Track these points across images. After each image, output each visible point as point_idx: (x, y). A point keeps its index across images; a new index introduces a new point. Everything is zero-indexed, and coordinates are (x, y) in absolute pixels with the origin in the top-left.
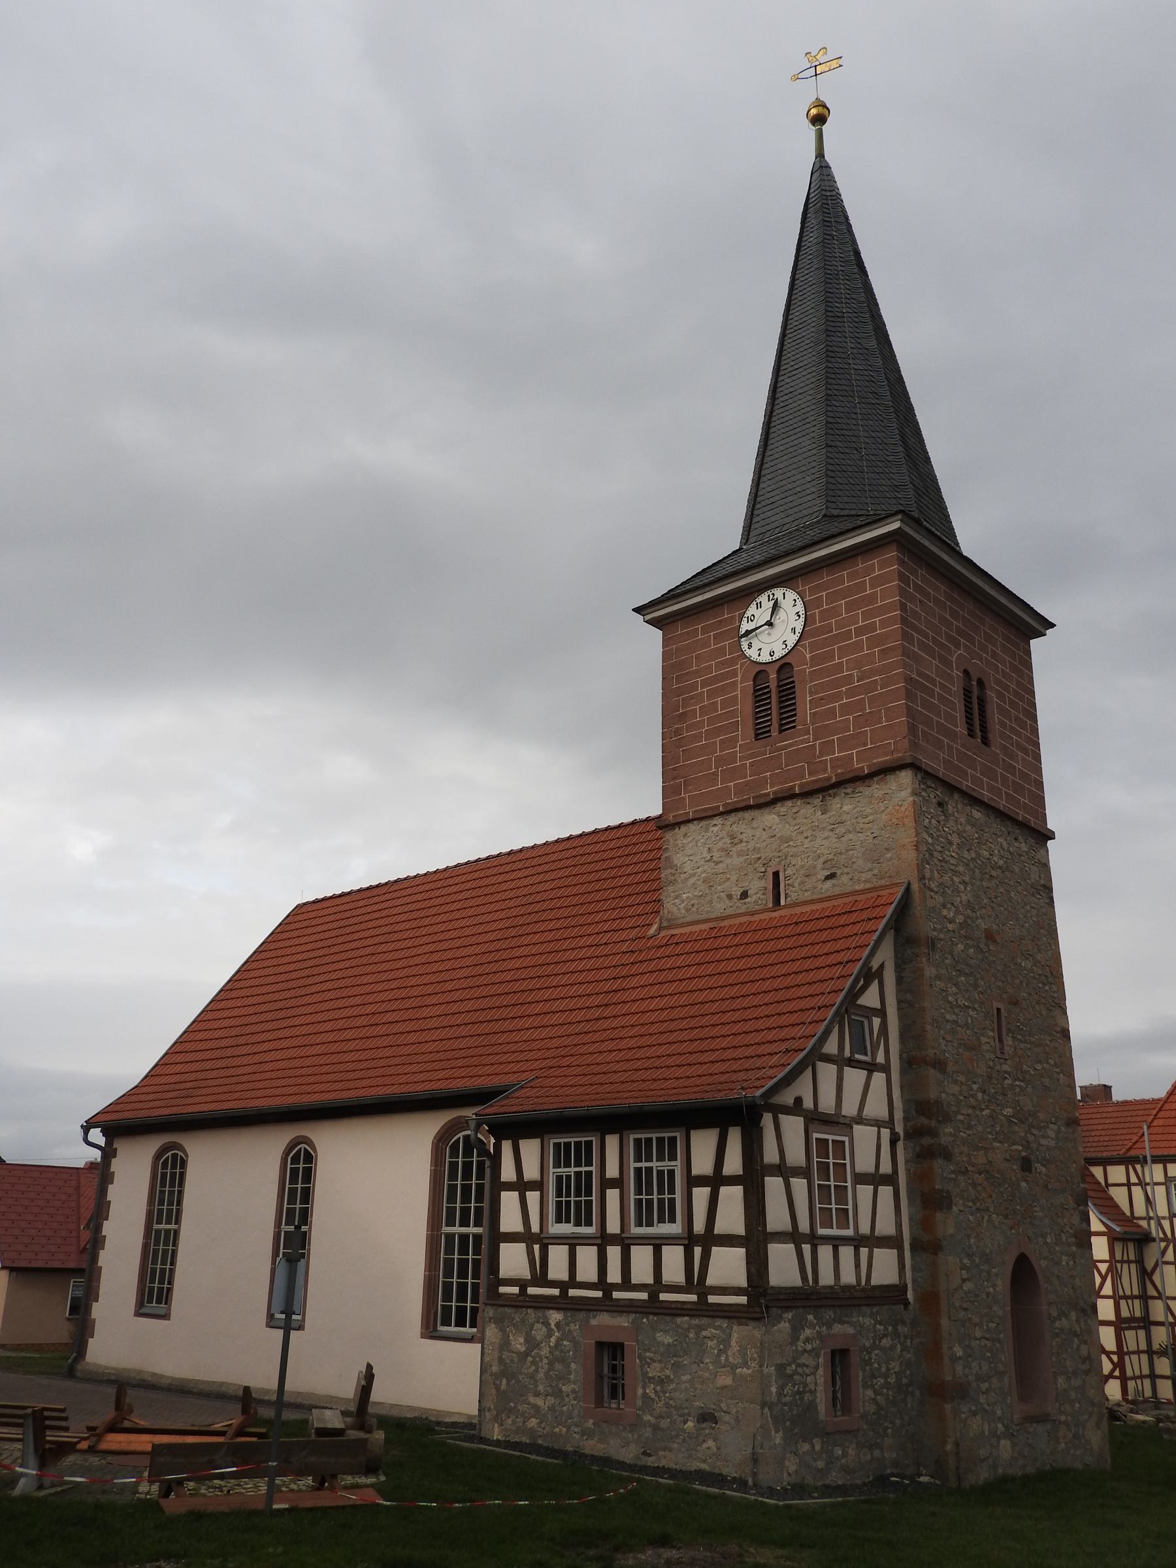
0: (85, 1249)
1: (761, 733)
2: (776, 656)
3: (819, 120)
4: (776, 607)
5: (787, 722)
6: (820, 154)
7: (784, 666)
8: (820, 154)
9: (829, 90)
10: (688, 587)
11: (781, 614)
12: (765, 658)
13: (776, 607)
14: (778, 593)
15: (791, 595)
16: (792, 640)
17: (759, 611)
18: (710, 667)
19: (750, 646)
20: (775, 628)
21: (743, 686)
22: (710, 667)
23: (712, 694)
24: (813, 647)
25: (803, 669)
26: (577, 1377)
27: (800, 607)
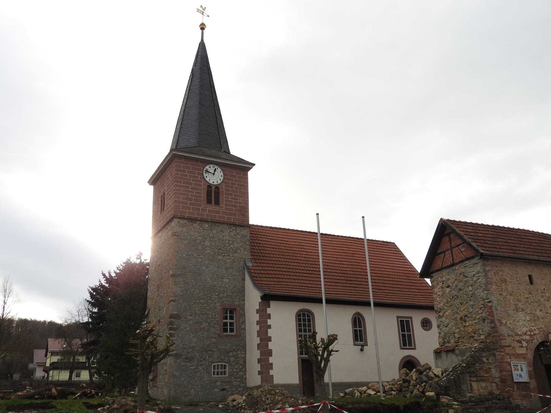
1: (209, 201)
2: (210, 182)
4: (215, 170)
5: (217, 203)
6: (202, 40)
7: (217, 187)
8: (202, 40)
12: (211, 182)
13: (215, 170)
16: (219, 182)
17: (211, 168)
18: (190, 167)
19: (207, 177)
25: (223, 190)
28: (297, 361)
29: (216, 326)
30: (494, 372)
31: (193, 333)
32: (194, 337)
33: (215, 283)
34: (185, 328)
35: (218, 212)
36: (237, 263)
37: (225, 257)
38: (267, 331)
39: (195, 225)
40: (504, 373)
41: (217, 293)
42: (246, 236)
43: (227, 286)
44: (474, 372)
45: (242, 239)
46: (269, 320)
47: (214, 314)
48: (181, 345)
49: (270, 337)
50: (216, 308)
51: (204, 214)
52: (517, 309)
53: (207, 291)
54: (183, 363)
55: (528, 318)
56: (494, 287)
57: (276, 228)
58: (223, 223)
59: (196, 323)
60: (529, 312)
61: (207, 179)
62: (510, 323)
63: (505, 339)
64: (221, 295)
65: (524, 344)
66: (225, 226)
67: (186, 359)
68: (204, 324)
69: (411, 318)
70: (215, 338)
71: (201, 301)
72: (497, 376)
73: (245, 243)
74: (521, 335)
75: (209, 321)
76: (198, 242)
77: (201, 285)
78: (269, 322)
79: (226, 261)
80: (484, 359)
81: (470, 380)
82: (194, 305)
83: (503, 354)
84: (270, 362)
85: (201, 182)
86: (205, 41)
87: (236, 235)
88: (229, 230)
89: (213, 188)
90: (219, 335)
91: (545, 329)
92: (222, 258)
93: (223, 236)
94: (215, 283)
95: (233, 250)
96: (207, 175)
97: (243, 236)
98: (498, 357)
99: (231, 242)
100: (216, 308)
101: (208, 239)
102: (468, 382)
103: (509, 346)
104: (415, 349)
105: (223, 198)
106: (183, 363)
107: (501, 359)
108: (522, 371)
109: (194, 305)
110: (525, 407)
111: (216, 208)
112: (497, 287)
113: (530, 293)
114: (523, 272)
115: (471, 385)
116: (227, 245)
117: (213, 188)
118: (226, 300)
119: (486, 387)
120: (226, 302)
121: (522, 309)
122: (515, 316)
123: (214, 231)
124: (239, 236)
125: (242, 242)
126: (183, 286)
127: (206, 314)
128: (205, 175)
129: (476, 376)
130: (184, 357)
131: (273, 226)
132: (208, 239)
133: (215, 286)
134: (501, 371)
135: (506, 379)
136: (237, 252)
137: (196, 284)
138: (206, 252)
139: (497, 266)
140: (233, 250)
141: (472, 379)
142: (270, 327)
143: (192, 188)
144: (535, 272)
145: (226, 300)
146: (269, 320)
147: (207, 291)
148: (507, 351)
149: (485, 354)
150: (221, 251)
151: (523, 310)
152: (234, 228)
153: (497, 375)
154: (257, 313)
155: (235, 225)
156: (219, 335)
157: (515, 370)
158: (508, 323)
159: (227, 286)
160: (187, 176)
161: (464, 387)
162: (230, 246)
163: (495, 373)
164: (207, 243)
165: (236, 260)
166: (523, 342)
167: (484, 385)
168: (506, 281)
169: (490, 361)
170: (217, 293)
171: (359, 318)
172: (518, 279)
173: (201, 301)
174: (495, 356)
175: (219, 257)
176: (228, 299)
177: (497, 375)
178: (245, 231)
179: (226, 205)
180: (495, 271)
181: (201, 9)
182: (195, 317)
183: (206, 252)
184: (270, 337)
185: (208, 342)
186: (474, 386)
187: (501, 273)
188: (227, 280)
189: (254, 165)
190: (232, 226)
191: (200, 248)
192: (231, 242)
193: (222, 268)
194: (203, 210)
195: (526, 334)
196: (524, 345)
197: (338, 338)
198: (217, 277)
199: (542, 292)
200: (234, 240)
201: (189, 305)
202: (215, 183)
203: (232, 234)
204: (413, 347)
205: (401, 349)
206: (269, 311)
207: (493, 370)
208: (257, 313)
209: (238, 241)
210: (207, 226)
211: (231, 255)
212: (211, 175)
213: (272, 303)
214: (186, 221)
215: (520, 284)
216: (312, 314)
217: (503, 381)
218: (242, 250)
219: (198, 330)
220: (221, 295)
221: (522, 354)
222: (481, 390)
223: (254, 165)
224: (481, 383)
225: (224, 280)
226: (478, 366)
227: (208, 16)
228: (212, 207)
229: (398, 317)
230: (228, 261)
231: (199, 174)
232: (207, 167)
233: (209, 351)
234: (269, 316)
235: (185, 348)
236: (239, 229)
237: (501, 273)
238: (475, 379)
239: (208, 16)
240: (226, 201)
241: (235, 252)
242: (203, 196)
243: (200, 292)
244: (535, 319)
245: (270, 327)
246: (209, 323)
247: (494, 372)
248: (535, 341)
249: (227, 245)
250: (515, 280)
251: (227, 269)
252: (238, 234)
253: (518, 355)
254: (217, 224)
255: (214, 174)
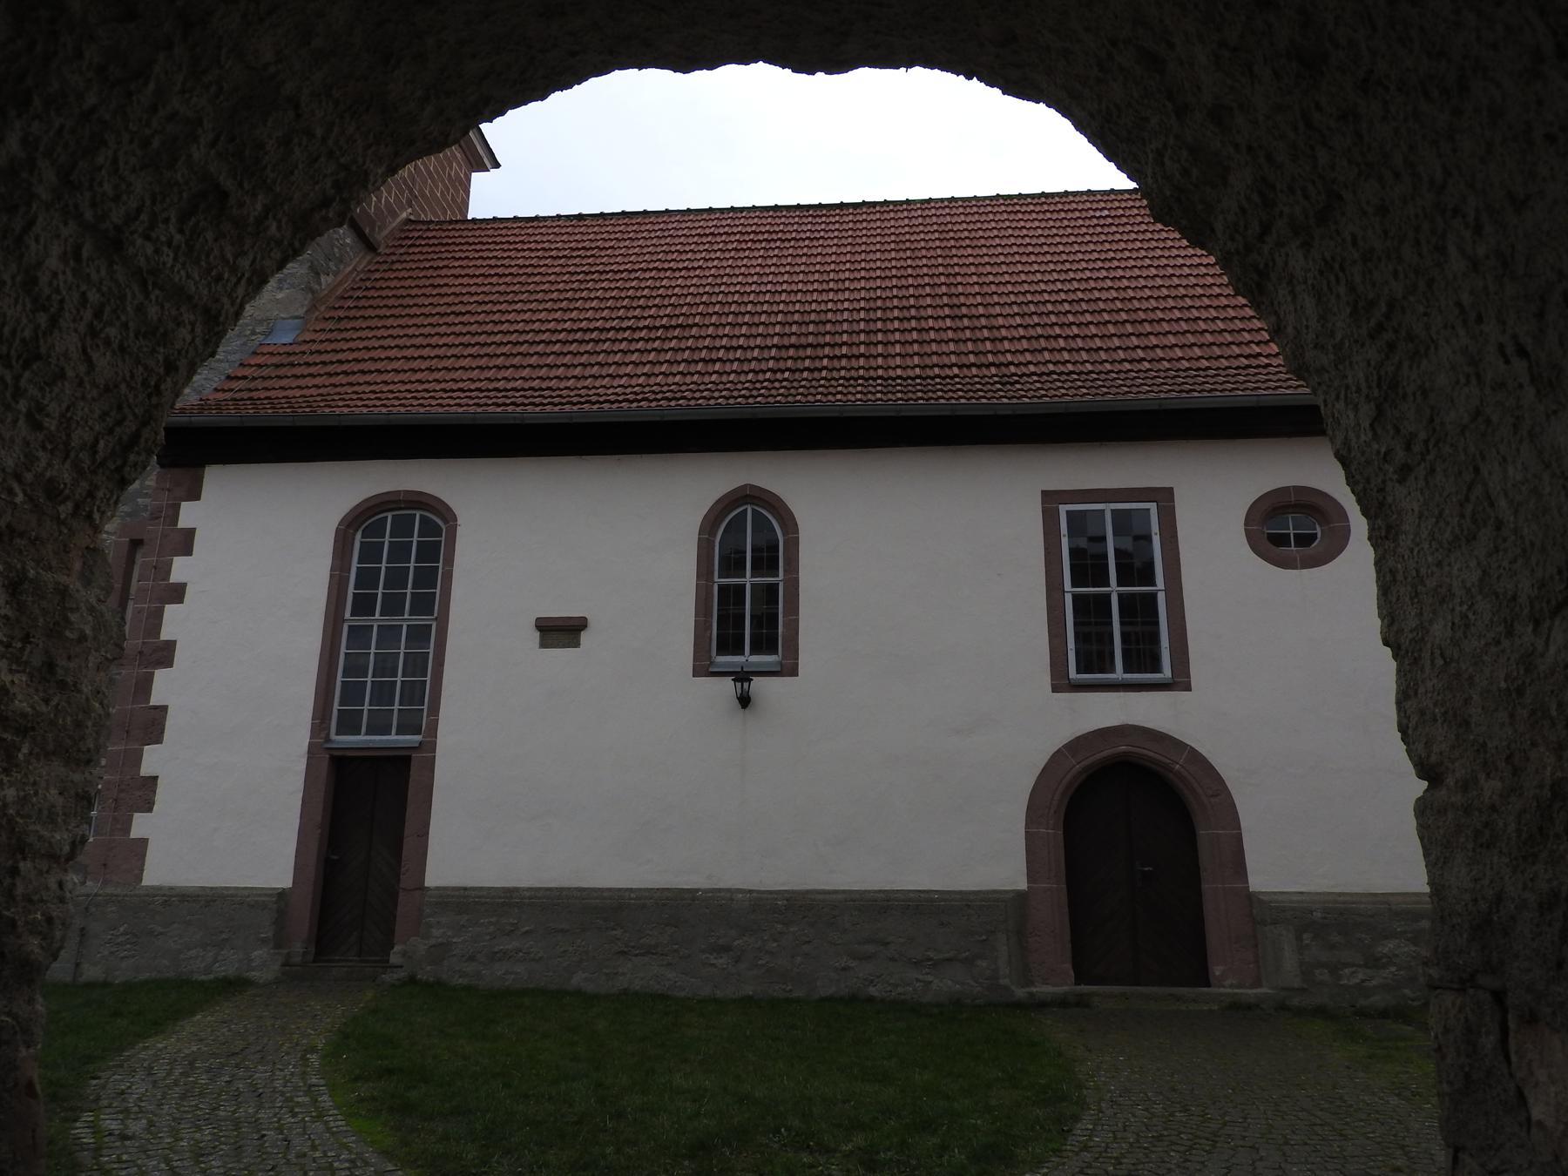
28: (302, 766)
38: (159, 614)
49: (171, 646)
57: (1023, 416)
69: (1164, 497)
78: (181, 569)
84: (146, 770)
104: (1180, 682)
131: (1373, 589)
142: (177, 593)
171: (761, 524)
184: (171, 646)
189: (497, 165)
197: (584, 637)
204: (1167, 672)
205: (1061, 683)
206: (189, 514)
213: (217, 480)
216: (449, 516)
223: (497, 165)
229: (1051, 499)
234: (185, 541)
245: (177, 593)
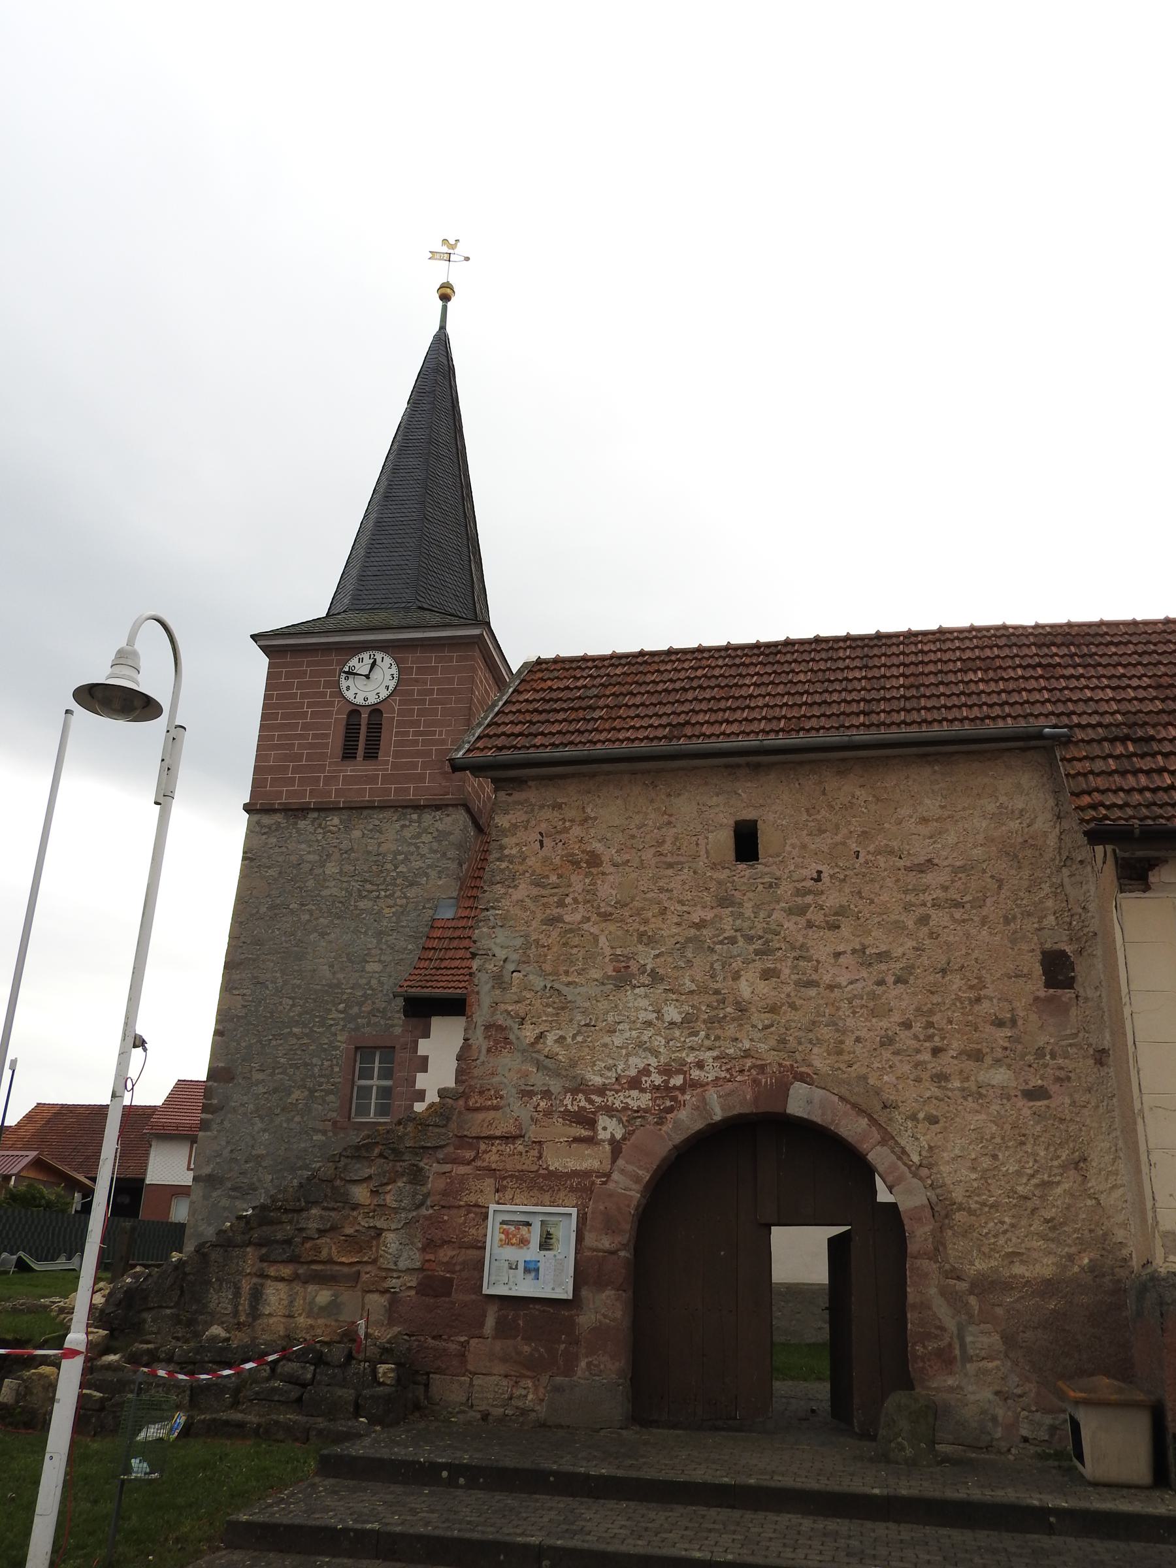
0: (982, 1105)
1: (349, 754)
2: (370, 702)
3: (445, 298)
4: (374, 664)
5: (372, 754)
6: (443, 327)
7: (376, 711)
8: (443, 327)
9: (457, 275)
10: (292, 631)
11: (377, 670)
12: (359, 700)
13: (374, 664)
14: (379, 656)
15: (388, 660)
16: (384, 694)
17: (359, 663)
18: (305, 672)
19: (348, 688)
20: (372, 682)
21: (339, 717)
22: (305, 672)
23: (303, 696)
24: (401, 702)
25: (391, 716)
26: (766, 839)
27: (394, 670)
29: (331, 1098)
30: (393, 1247)
31: (261, 1118)
32: (264, 1131)
33: (340, 976)
34: (242, 1105)
35: (373, 779)
36: (413, 915)
37: (381, 903)
39: (302, 824)
40: (445, 1254)
41: (342, 1006)
42: (450, 833)
43: (374, 982)
44: (288, 1242)
45: (435, 845)
46: (420, 1076)
47: (326, 1063)
48: (226, 1153)
50: (336, 1048)
51: (330, 792)
52: (622, 978)
53: (315, 1001)
54: (225, 1202)
55: (673, 1013)
56: (523, 891)
58: (382, 808)
59: (275, 1090)
60: (690, 985)
61: (349, 695)
62: (561, 1040)
63: (496, 1108)
64: (356, 1010)
65: (609, 1128)
66: (388, 814)
67: (234, 1189)
68: (297, 1094)
70: (324, 1133)
71: (295, 1030)
72: (403, 1264)
73: (444, 854)
74: (602, 1091)
75: (310, 1084)
76: (306, 867)
77: (299, 987)
79: (380, 912)
80: (360, 1194)
81: (263, 1276)
82: (274, 1043)
83: (462, 1170)
85: (331, 704)
86: (449, 329)
87: (419, 836)
88: (397, 826)
89: (365, 716)
90: (335, 1123)
91: (771, 1057)
92: (370, 904)
93: (379, 844)
94: (340, 976)
95: (405, 879)
96: (350, 682)
97: (442, 836)
98: (434, 1184)
99: (401, 857)
100: (336, 1048)
101: (336, 856)
102: (246, 1286)
103: (507, 1138)
105: (390, 739)
106: (225, 1202)
107: (445, 1193)
108: (546, 1243)
109: (274, 1043)
110: (524, 1412)
111: (368, 768)
112: (535, 891)
113: (724, 901)
114: (703, 815)
115: (257, 1295)
116: (389, 866)
117: (365, 716)
118: (368, 1024)
119: (332, 1308)
120: (367, 1029)
121: (654, 974)
122: (603, 1005)
123: (356, 834)
124: (426, 838)
125: (436, 852)
126: (248, 992)
127: (306, 1064)
128: (344, 684)
129: (294, 1260)
130: (229, 1185)
132: (336, 856)
133: (338, 985)
134: (430, 1245)
135: (450, 1284)
136: (419, 884)
137: (285, 983)
138: (325, 893)
139: (558, 806)
140: (405, 879)
141: (272, 1271)
143: (305, 727)
144: (777, 807)
145: (368, 1024)
146: (420, 1076)
147: (315, 1001)
148: (492, 1158)
149: (367, 1172)
150: (368, 886)
151: (656, 978)
152: (415, 817)
153: (411, 1258)
154: (426, 1058)
155: (417, 807)
156: (335, 1123)
157: (507, 1241)
158: (551, 1038)
159: (374, 982)
160: (324, 695)
161: (220, 1300)
162: (396, 868)
163: (398, 1250)
164: (331, 868)
165: (411, 906)
166: (603, 1121)
167: (324, 1296)
168: (594, 860)
169: (389, 1199)
170: (342, 1006)
172: (667, 847)
173: (295, 1030)
174: (417, 1176)
175: (361, 905)
176: (374, 1020)
177: (411, 1258)
178: (448, 820)
179: (397, 754)
180: (544, 827)
181: (445, 249)
182: (272, 1074)
183: (325, 893)
185: (303, 1145)
186: (273, 1299)
187: (576, 831)
188: (376, 967)
190: (409, 810)
191: (311, 884)
192: (401, 857)
193: (366, 933)
194: (328, 780)
195: (634, 1084)
196: (603, 1135)
198: (350, 960)
199: (799, 893)
200: (412, 849)
201: (260, 1042)
202: (372, 700)
203: (407, 833)
207: (391, 1240)
208: (426, 1058)
209: (424, 850)
210: (336, 821)
211: (398, 894)
212: (360, 682)
214: (278, 818)
215: (670, 866)
217: (433, 1286)
218: (433, 874)
219: (278, 1111)
220: (356, 1010)
221: (575, 1173)
222: (301, 1320)
224: (311, 1288)
225: (369, 967)
226: (314, 1218)
227: (467, 259)
228: (358, 768)
230: (387, 910)
231: (328, 684)
232: (354, 662)
233: (300, 1168)
235: (235, 1160)
236: (427, 818)
237: (576, 831)
238: (286, 1271)
239: (467, 259)
240: (399, 743)
241: (411, 885)
242: (334, 740)
243: (293, 1005)
244: (719, 1012)
246: (312, 1091)
247: (393, 1247)
248: (683, 1114)
249: (389, 866)
250: (648, 855)
251: (379, 934)
252: (426, 831)
253: (555, 1176)
254: (365, 813)
255: (367, 677)
